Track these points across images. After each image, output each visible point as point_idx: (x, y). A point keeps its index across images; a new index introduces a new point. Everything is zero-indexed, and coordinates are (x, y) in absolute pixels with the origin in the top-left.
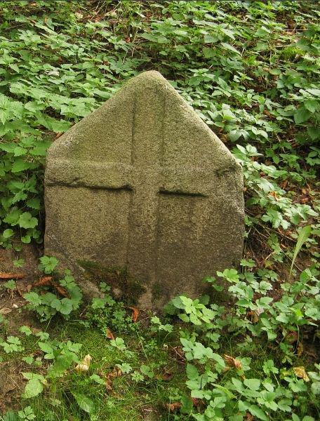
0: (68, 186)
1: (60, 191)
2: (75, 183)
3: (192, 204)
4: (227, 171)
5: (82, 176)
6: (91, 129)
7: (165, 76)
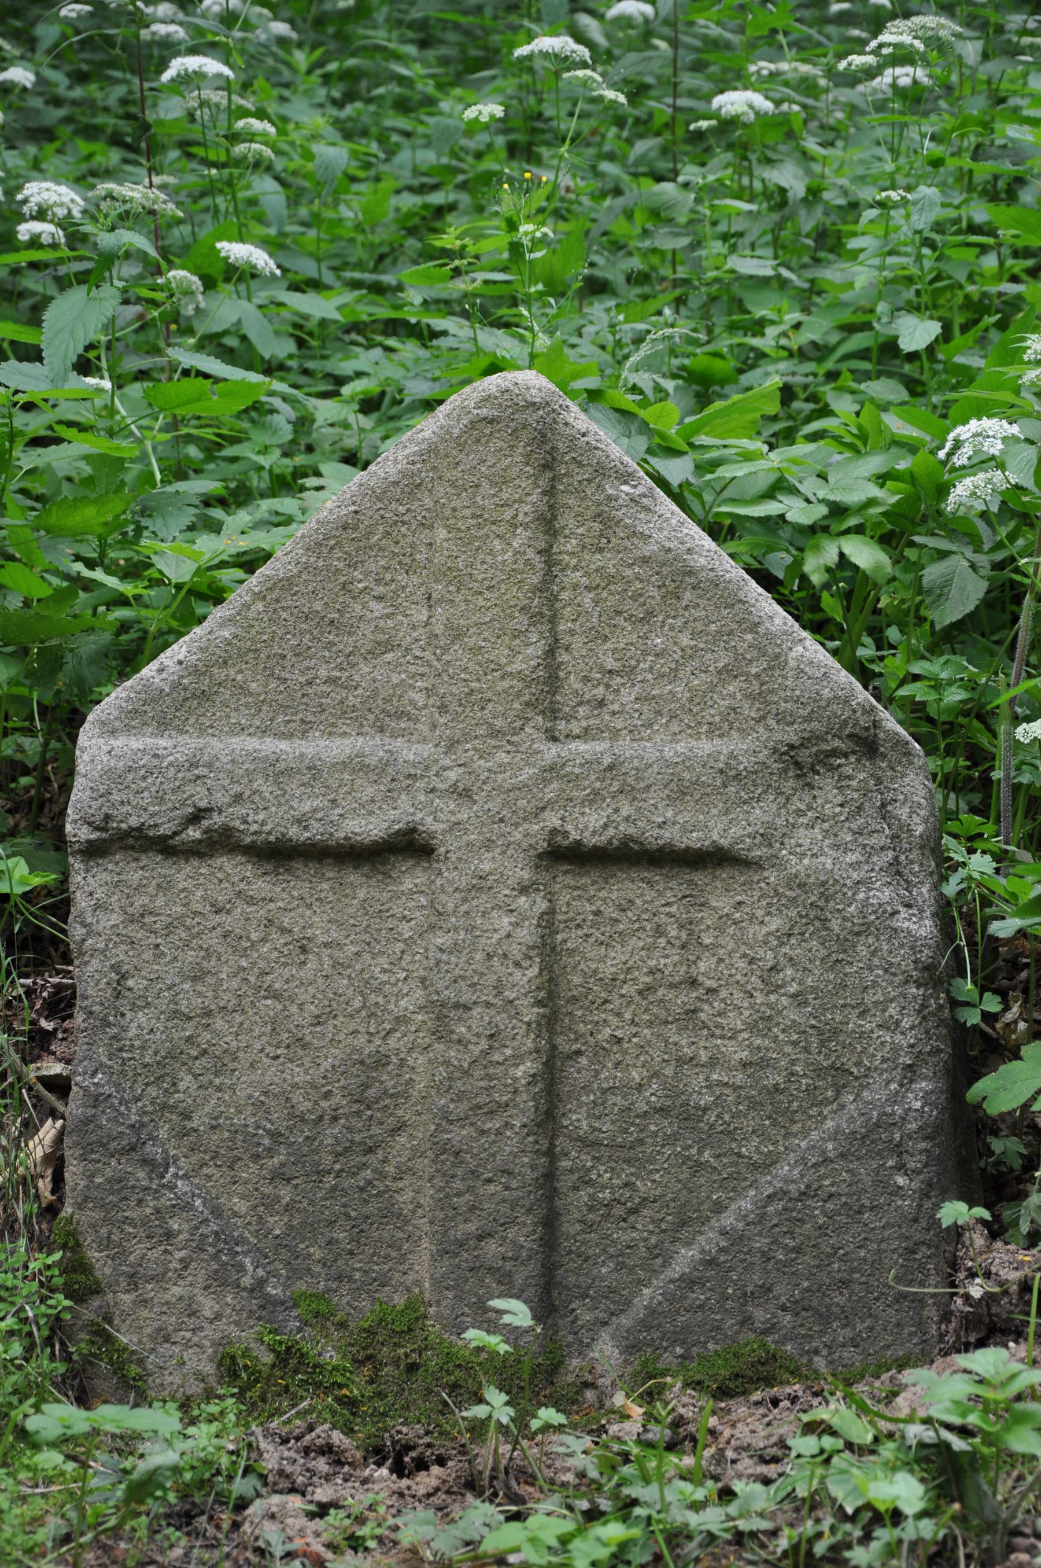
0: (166, 847)
1: (135, 876)
2: (194, 833)
3: (696, 901)
4: (834, 753)
5: (221, 798)
6: (260, 606)
7: (123, 676)
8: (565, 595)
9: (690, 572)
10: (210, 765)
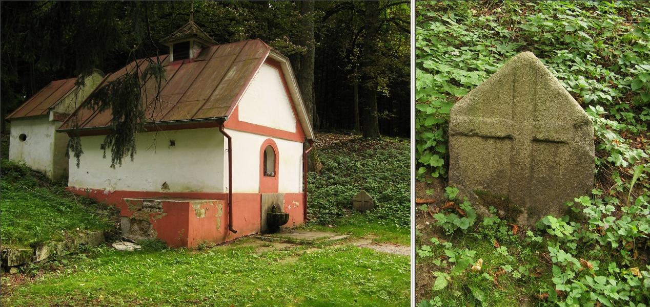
0: (466, 135)
2: (471, 133)
4: (582, 125)
5: (476, 128)
7: (537, 56)
8: (537, 96)
9: (559, 93)
10: (474, 122)
